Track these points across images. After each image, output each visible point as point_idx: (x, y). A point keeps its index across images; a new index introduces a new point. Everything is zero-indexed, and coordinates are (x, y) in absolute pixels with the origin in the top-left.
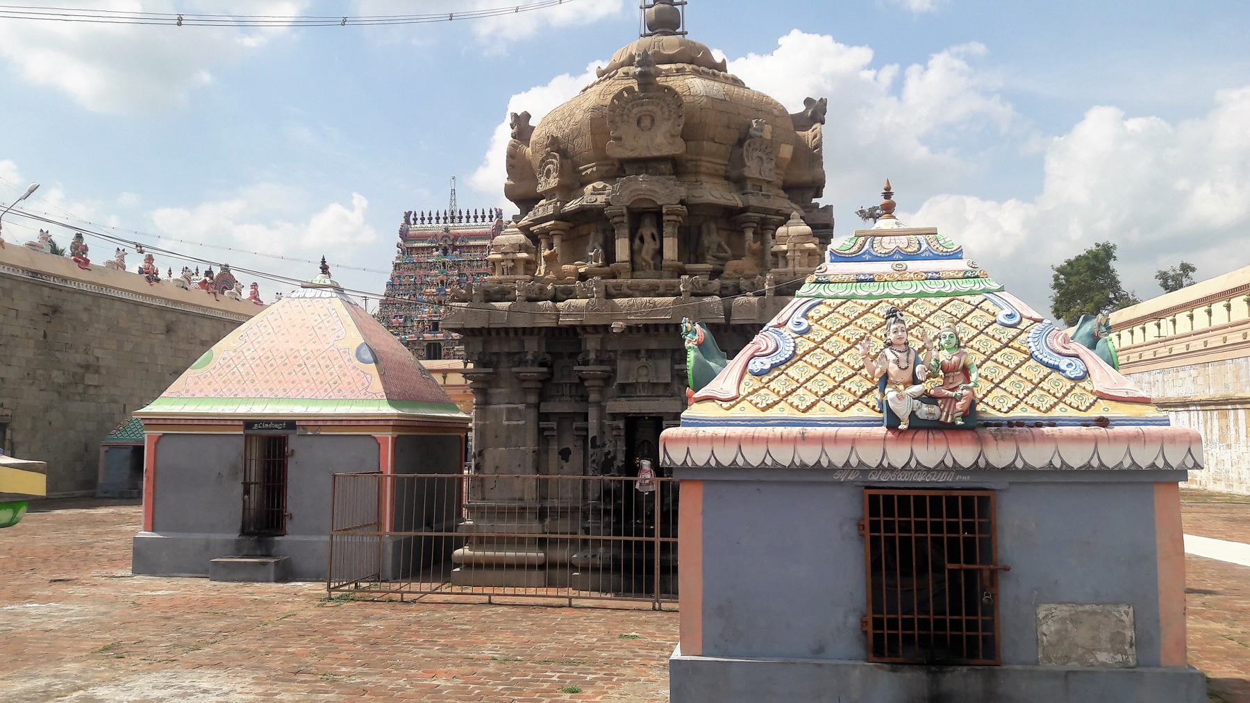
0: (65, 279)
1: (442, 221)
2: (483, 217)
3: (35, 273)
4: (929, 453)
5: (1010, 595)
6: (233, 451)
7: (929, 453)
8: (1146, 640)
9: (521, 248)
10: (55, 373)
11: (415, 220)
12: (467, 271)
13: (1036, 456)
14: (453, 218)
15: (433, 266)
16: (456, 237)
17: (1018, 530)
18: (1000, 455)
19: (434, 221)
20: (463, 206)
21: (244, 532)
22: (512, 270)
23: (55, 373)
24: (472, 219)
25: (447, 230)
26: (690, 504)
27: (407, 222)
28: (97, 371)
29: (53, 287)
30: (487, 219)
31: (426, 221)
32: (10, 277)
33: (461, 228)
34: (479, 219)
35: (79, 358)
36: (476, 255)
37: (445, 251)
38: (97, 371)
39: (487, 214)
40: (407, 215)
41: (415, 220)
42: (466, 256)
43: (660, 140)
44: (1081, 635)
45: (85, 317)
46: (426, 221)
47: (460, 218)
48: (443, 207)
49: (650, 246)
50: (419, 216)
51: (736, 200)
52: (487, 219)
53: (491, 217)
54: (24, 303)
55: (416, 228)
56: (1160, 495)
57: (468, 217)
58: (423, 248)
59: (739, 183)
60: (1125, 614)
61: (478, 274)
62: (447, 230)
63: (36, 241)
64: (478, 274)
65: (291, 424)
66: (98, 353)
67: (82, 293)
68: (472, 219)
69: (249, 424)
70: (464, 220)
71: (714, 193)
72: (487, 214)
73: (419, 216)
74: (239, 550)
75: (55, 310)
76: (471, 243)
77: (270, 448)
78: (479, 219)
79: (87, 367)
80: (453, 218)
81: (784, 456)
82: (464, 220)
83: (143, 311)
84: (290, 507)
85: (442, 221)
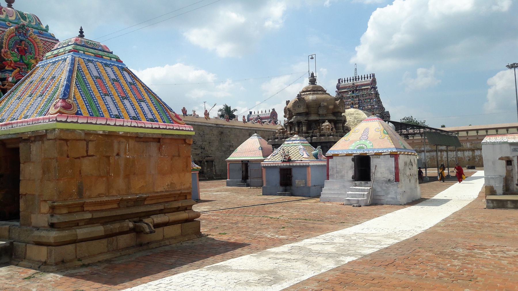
0: (224, 125)
1: (352, 81)
2: (367, 77)
3: (217, 125)
4: (285, 164)
5: (293, 179)
6: (240, 165)
7: (285, 164)
8: (306, 183)
9: (281, 129)
10: (223, 148)
11: (342, 81)
12: (361, 98)
13: (295, 164)
14: (356, 79)
15: (349, 98)
16: (357, 86)
17: (294, 172)
18: (291, 164)
19: (349, 81)
20: (359, 74)
21: (243, 179)
22: (280, 134)
23: (223, 148)
24: (363, 79)
25: (353, 84)
26: (264, 171)
27: (339, 82)
28: (233, 147)
29: (221, 127)
30: (369, 78)
31: (346, 81)
32: (212, 126)
33: (359, 82)
34: (366, 78)
35: (228, 144)
36: (365, 92)
37: (353, 92)
38: (233, 147)
39: (369, 76)
40: (339, 80)
41: (342, 81)
42: (361, 93)
43: (302, 110)
44: (300, 183)
45: (229, 134)
46: (346, 81)
47: (359, 79)
48: (352, 75)
49: (301, 128)
50: (343, 80)
51: (318, 118)
52: (369, 78)
53: (370, 77)
54: (215, 132)
55: (343, 84)
56: (307, 168)
57: (362, 78)
58: (345, 92)
59: (319, 115)
60: (304, 181)
61: (366, 99)
62: (353, 84)
63: (217, 116)
64: (366, 99)
65: (248, 161)
66: (233, 142)
67: (228, 128)
68: (363, 79)
69: (242, 161)
70: (360, 79)
71: (313, 117)
72: (369, 76)
73: (343, 80)
74: (242, 182)
75: (222, 133)
76: (363, 88)
77: (246, 164)
78: (366, 78)
79: (230, 146)
80: (356, 79)
81: (272, 165)
82: (360, 79)
83: (243, 131)
84: (249, 175)
85: (352, 81)
